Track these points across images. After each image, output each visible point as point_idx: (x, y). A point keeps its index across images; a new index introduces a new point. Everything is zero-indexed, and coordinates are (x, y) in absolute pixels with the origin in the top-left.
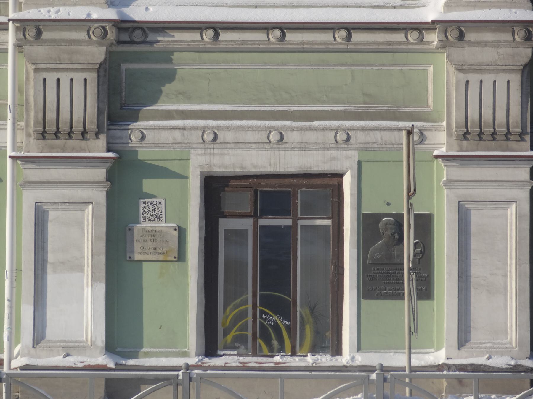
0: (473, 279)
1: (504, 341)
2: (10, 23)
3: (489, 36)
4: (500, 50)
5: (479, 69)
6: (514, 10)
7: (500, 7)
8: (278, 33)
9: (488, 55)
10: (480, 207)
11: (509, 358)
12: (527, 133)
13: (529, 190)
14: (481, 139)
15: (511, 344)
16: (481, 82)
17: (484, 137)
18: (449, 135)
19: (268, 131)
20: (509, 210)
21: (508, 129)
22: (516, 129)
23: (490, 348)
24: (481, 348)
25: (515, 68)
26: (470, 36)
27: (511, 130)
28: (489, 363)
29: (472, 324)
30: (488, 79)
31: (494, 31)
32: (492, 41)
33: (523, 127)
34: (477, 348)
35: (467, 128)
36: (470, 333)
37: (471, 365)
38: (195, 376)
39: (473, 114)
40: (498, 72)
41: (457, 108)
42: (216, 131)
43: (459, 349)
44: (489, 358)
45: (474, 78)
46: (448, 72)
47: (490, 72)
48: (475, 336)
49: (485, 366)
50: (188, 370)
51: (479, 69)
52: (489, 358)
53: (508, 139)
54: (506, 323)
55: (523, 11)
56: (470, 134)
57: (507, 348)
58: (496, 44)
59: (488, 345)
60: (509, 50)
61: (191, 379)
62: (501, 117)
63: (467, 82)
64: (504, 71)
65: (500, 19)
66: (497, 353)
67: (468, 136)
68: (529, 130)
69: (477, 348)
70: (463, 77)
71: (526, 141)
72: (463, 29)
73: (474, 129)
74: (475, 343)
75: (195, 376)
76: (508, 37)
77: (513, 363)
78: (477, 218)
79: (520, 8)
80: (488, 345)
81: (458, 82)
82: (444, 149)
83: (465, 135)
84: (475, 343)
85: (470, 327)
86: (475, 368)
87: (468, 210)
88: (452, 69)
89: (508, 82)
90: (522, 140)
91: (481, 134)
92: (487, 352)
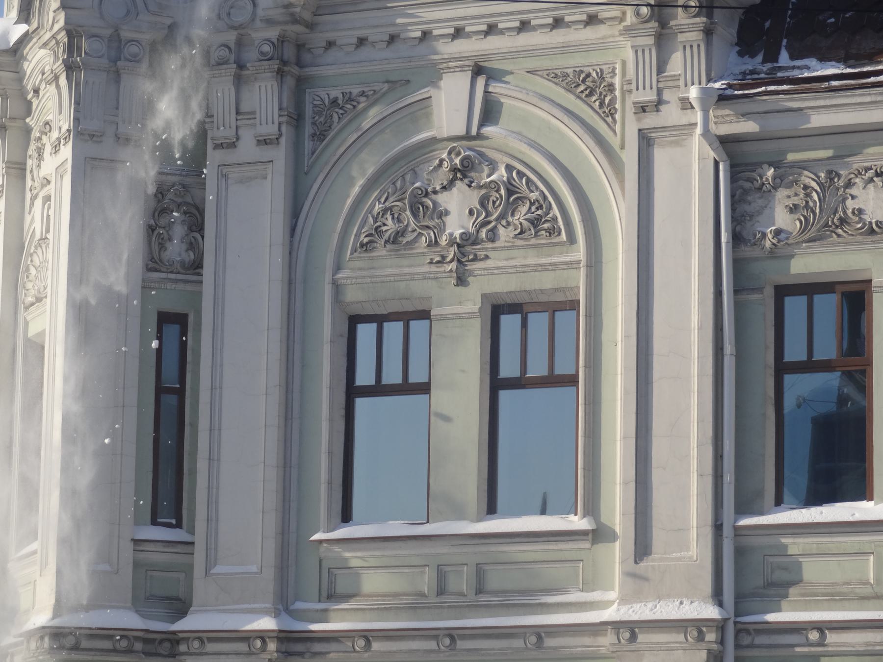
72: (704, 629)
76: (432, 645)
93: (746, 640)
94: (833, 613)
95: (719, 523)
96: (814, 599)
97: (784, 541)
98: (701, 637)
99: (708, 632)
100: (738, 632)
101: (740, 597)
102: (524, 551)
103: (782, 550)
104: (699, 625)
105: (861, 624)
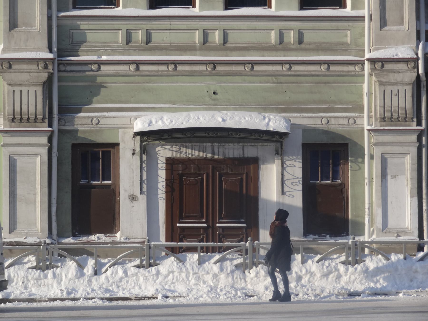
0: (18, 196)
1: (34, 229)
2: (366, 62)
3: (25, 67)
4: (31, 74)
5: (20, 84)
6: (39, 53)
7: (32, 51)
8: (173, 66)
9: (24, 77)
10: (22, 158)
11: (37, 238)
12: (46, 118)
13: (47, 149)
14: (21, 122)
15: (38, 231)
16: (21, 91)
17: (23, 121)
18: (5, 119)
19: (321, 119)
20: (406, 158)
21: (36, 116)
22: (40, 116)
23: (27, 233)
24: (22, 233)
25: (39, 83)
26: (15, 67)
27: (37, 117)
28: (25, 241)
29: (18, 220)
30: (25, 90)
31: (27, 64)
32: (27, 69)
33: (44, 115)
34: (19, 233)
35: (14, 116)
36: (16, 225)
37: (16, 242)
38: (152, 246)
39: (17, 108)
40: (30, 85)
41: (9, 105)
42: (356, 119)
43: (10, 233)
44: (25, 238)
45: (17, 89)
46: (4, 86)
47: (26, 86)
48: (19, 226)
49: (23, 242)
50: (148, 242)
51: (20, 84)
52: (25, 238)
53: (36, 122)
54: (35, 220)
55: (44, 53)
56: (15, 119)
57: (36, 233)
58: (29, 71)
59: (26, 231)
60: (36, 74)
61: (150, 248)
62: (32, 110)
63: (14, 91)
64: (33, 85)
65: (31, 57)
66: (30, 236)
67: (15, 120)
68: (47, 117)
69: (19, 233)
70: (383, 88)
71: (45, 122)
72: (11, 63)
73: (17, 116)
74: (19, 230)
75: (152, 246)
76: (35, 67)
77: (38, 241)
78: (20, 164)
79: (42, 51)
80: (26, 231)
81: (8, 91)
82: (2, 127)
83: (13, 120)
84: (19, 230)
85: (16, 222)
86: (18, 244)
87: (15, 160)
88: (6, 84)
89: (36, 91)
90: (43, 122)
91: (21, 119)
92: (25, 235)
93: (62, 68)
94: (155, 56)
95: (49, 15)
96: (89, 52)
97: (79, 23)
98: (46, 67)
99: (50, 65)
100: (59, 64)
101: (59, 50)
102: (178, 24)
103: (78, 28)
104: (45, 60)
105: (237, 62)
